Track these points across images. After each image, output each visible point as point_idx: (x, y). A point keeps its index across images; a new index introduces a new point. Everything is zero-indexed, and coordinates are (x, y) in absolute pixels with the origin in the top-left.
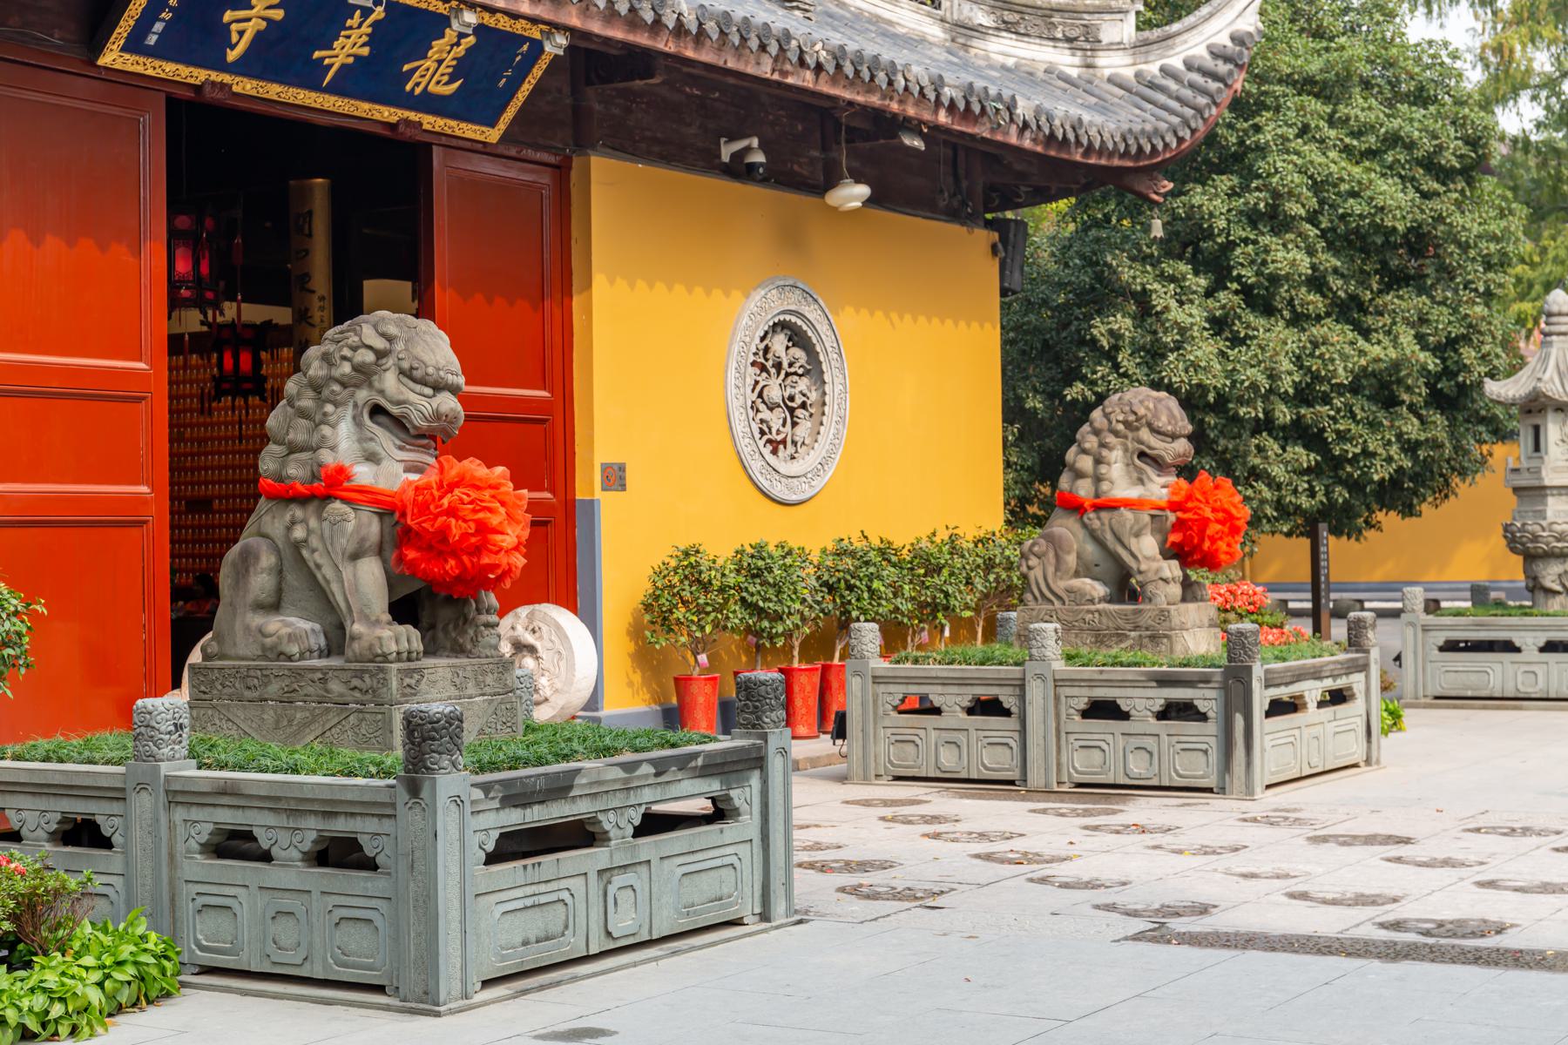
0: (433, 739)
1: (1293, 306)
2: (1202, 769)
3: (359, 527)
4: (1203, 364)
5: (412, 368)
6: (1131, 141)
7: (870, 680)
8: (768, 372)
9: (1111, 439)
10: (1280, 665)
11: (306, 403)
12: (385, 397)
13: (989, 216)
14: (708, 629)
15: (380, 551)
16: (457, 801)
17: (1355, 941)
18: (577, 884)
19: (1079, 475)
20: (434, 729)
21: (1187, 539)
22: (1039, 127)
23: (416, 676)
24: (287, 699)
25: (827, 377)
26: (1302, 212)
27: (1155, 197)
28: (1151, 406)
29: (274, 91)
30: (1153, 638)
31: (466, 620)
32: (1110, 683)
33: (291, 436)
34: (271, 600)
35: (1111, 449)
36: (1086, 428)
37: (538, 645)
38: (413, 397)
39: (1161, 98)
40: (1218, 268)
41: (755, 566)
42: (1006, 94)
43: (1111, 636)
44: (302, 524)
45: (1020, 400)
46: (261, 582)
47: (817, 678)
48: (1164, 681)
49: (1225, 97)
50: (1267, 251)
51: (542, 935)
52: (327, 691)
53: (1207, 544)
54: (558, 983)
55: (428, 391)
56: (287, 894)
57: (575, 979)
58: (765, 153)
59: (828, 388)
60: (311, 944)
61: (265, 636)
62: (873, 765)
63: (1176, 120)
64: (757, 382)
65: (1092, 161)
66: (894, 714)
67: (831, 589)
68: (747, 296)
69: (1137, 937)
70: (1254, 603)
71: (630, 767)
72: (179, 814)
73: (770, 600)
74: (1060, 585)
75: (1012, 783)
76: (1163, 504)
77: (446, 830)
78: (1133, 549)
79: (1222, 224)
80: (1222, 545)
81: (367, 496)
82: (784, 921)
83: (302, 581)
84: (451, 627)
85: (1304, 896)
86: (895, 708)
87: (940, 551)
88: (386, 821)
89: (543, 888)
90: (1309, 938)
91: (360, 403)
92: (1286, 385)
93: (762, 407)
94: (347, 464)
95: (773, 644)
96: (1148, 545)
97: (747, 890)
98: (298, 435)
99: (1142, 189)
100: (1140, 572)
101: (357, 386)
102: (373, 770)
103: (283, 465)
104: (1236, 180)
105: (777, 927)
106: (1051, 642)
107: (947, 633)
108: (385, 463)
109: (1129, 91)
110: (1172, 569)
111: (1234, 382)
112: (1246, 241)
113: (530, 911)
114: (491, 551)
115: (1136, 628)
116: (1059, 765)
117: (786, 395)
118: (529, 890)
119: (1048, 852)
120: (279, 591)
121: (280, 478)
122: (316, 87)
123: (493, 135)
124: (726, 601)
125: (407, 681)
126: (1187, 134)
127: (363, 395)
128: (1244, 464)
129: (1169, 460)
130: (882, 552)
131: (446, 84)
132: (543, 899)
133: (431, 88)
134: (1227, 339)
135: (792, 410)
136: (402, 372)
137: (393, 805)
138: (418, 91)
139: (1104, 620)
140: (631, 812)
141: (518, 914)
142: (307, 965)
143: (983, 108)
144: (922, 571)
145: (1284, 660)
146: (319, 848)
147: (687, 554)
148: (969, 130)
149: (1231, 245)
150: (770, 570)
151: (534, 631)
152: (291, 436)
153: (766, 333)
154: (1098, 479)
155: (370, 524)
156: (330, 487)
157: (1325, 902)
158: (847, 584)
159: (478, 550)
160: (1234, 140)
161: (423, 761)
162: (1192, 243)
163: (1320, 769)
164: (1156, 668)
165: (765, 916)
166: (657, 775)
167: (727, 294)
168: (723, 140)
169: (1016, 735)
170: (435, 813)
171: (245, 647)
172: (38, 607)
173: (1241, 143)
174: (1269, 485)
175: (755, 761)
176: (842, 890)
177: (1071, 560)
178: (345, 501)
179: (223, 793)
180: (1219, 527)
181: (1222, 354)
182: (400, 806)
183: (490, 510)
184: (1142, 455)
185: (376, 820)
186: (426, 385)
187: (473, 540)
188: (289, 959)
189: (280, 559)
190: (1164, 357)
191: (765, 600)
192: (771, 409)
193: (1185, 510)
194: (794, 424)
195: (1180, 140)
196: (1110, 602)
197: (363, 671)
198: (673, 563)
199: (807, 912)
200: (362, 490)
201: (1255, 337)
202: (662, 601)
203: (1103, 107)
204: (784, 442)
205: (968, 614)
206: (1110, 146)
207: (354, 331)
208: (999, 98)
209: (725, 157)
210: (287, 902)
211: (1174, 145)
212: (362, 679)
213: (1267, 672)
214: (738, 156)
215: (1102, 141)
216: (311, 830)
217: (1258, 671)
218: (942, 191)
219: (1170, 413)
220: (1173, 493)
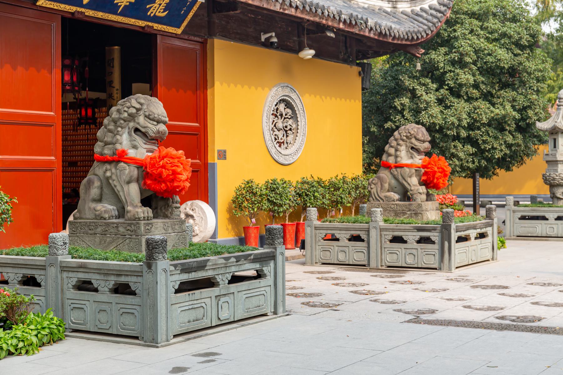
0: (156, 248)
2: (433, 261)
3: (130, 172)
4: (435, 115)
5: (149, 115)
6: (409, 35)
7: (314, 228)
9: (401, 142)
10: (461, 224)
11: (111, 127)
13: (358, 62)
14: (256, 210)
15: (137, 181)
16: (165, 271)
17: (487, 323)
18: (208, 301)
19: (389, 155)
20: (157, 245)
22: (376, 29)
23: (150, 226)
24: (104, 234)
25: (299, 119)
26: (471, 61)
27: (418, 55)
29: (100, 15)
30: (416, 214)
32: (400, 230)
34: (98, 198)
35: (401, 146)
36: (392, 138)
37: (194, 215)
40: (440, 81)
41: (272, 187)
42: (364, 17)
43: (401, 213)
44: (109, 171)
45: (369, 128)
46: (95, 192)
47: (294, 228)
48: (419, 229)
49: (444, 19)
50: (458, 75)
51: (195, 319)
52: (118, 231)
53: (435, 181)
54: (201, 336)
55: (155, 123)
56: (104, 304)
57: (207, 335)
59: (299, 123)
60: (112, 322)
61: (96, 211)
63: (426, 27)
64: (274, 121)
65: (395, 42)
66: (322, 241)
67: (300, 195)
68: (270, 90)
69: (409, 321)
70: (452, 202)
71: (227, 259)
72: (65, 275)
73: (278, 199)
74: (382, 195)
75: (364, 266)
76: (420, 166)
79: (442, 65)
80: (441, 181)
81: (133, 161)
82: (282, 314)
83: (109, 191)
84: (163, 208)
85: (469, 307)
86: (323, 238)
87: (339, 182)
88: (139, 278)
89: (195, 302)
90: (471, 322)
91: (131, 127)
92: (465, 123)
93: (275, 130)
96: (414, 181)
97: (269, 303)
98: (108, 139)
99: (413, 52)
100: (411, 190)
101: (130, 121)
103: (103, 149)
104: (447, 49)
105: (280, 317)
107: (341, 212)
108: (139, 149)
109: (409, 16)
110: (423, 189)
111: (446, 122)
112: (450, 71)
113: (191, 311)
115: (410, 210)
116: (381, 259)
118: (191, 303)
119: (377, 291)
120: (101, 195)
123: (179, 31)
124: (262, 199)
125: (147, 227)
126: (429, 32)
127: (132, 124)
128: (449, 152)
129: (422, 150)
130: (318, 182)
131: (162, 12)
132: (195, 306)
133: (157, 14)
134: (443, 106)
135: (286, 131)
136: (146, 116)
137: (142, 272)
138: (152, 15)
139: (398, 207)
140: (227, 275)
143: (356, 22)
144: (333, 189)
145: (463, 222)
146: (115, 287)
147: (248, 183)
148: (351, 30)
149: (445, 73)
150: (278, 189)
151: (193, 210)
152: (106, 139)
153: (277, 103)
154: (396, 157)
155: (134, 171)
156: (120, 157)
157: (477, 309)
158: (306, 194)
159: (173, 181)
161: (153, 256)
164: (417, 225)
165: (275, 313)
166: (237, 262)
167: (263, 89)
168: (262, 33)
169: (366, 249)
173: (449, 36)
174: (458, 160)
175: (272, 257)
176: (303, 303)
177: (386, 186)
179: (81, 267)
180: (440, 174)
181: (442, 112)
182: (144, 272)
183: (177, 166)
185: (136, 277)
187: (171, 177)
188: (104, 327)
190: (421, 113)
191: (276, 199)
192: (279, 131)
193: (428, 168)
194: (287, 136)
195: (427, 35)
196: (400, 201)
197: (132, 224)
198: (243, 186)
199: (290, 311)
200: (131, 159)
201: (452, 106)
203: (399, 22)
204: (283, 142)
205: (349, 205)
206: (402, 37)
208: (362, 19)
209: (263, 39)
210: (104, 307)
211: (425, 36)
213: (457, 226)
214: (267, 39)
216: (112, 281)
217: (453, 226)
218: (341, 52)
219: (422, 133)
220: (423, 162)
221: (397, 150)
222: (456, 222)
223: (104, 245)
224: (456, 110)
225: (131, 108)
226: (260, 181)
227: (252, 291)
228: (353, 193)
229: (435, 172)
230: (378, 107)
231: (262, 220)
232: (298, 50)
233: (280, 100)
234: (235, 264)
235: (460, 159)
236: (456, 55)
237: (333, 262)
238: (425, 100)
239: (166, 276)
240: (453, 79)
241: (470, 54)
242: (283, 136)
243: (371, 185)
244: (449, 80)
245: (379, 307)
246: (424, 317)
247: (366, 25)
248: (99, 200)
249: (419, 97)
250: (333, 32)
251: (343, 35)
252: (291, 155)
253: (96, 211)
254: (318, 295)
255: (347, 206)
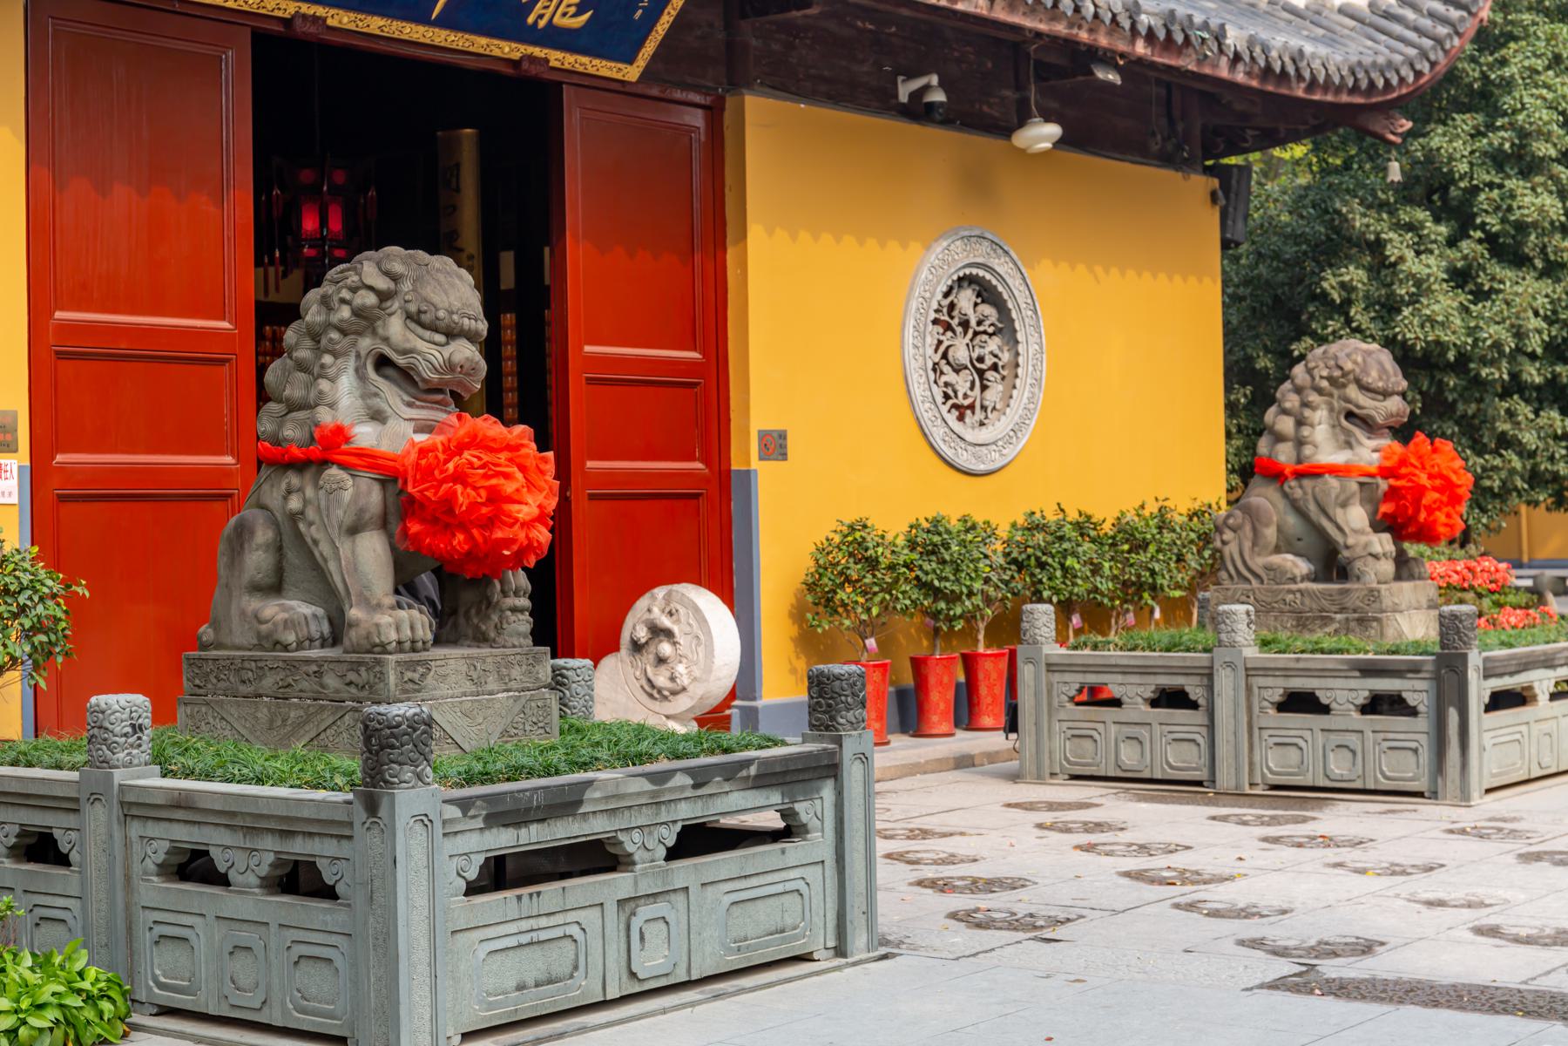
0: (392, 747)
1: (1546, 254)
2: (1411, 770)
3: (356, 496)
4: (1440, 318)
5: (420, 312)
6: (1361, 75)
7: (1044, 668)
8: (954, 331)
9: (1313, 397)
10: (1505, 652)
11: (303, 353)
12: (389, 346)
13: (1210, 163)
14: (875, 611)
15: (384, 524)
16: (424, 820)
17: (1539, 994)
18: (591, 917)
19: (1279, 438)
20: (393, 735)
21: (1400, 509)
22: (1252, 58)
23: (421, 670)
24: (282, 695)
25: (1020, 336)
26: (1553, 153)
27: (1392, 137)
28: (1359, 359)
29: (374, 24)
30: (1362, 621)
31: (489, 604)
32: (1307, 672)
33: (287, 392)
34: (269, 581)
35: (1314, 408)
36: (1287, 385)
37: (676, 629)
38: (422, 346)
39: (1397, 28)
40: (1461, 218)
41: (931, 542)
42: (1214, 23)
43: (1315, 618)
44: (285, 494)
45: (1250, 360)
46: (257, 561)
47: (1003, 664)
48: (1369, 670)
49: (1470, 27)
50: (1513, 196)
51: (543, 977)
52: (323, 686)
53: (1423, 516)
54: (561, 1035)
55: (440, 338)
56: (245, 925)
57: (584, 1030)
58: (947, 92)
59: (1021, 348)
60: (269, 987)
61: (261, 622)
62: (1047, 762)
63: (1412, 52)
64: (940, 342)
65: (1317, 97)
66: (1070, 706)
67: (1021, 566)
68: (928, 248)
69: (1274, 986)
70: (1495, 582)
71: (660, 778)
72: (135, 829)
73: (947, 579)
74: (1258, 562)
75: (1199, 783)
76: (1373, 470)
77: (408, 855)
78: (1340, 521)
79: (1463, 167)
80: (1441, 517)
81: (368, 461)
82: (864, 956)
83: (297, 563)
84: (473, 611)
85: (1493, 932)
86: (1072, 699)
87: (1147, 525)
88: (344, 843)
89: (543, 922)
90: (1484, 989)
91: (363, 353)
92: (1535, 344)
93: (946, 369)
94: (346, 423)
95: (951, 628)
96: (1356, 517)
97: (818, 920)
98: (294, 391)
99: (1377, 128)
100: (1347, 547)
101: (359, 334)
102: (339, 780)
103: (281, 426)
104: (1480, 118)
105: (854, 964)
106: (1242, 626)
107: (1157, 615)
108: (391, 422)
109: (1361, 21)
110: (1383, 543)
111: (1476, 340)
112: (1491, 185)
113: (527, 950)
114: (505, 524)
115: (1342, 610)
116: (1251, 764)
117: (975, 356)
118: (525, 925)
119: (1209, 869)
120: (279, 571)
121: (276, 441)
122: (423, 19)
123: (632, 73)
124: (896, 581)
125: (409, 675)
126: (1426, 68)
127: (366, 343)
128: (1494, 429)
129: (1380, 420)
130: (1078, 526)
131: (574, 16)
132: (543, 936)
133: (556, 20)
134: (1471, 292)
135: (981, 373)
136: (409, 316)
137: (351, 824)
138: (542, 23)
139: (1307, 601)
140: (663, 831)
141: (511, 953)
142: (266, 1010)
143: (1187, 38)
144: (1126, 547)
145: (1511, 646)
146: (279, 872)
147: (852, 528)
148: (1173, 62)
149: (1475, 190)
150: (947, 547)
151: (671, 614)
152: (287, 392)
153: (951, 289)
154: (1300, 443)
155: (369, 492)
156: (329, 450)
157: (1517, 940)
158: (1038, 558)
159: (491, 522)
160: (1477, 75)
161: (381, 773)
162: (1433, 189)
163: (1553, 770)
164: (1361, 656)
165: (840, 951)
166: (696, 786)
167: (904, 246)
168: (900, 78)
169: (1204, 731)
170: (394, 835)
171: (241, 634)
172: (80, 590)
173: (1485, 76)
174: (1520, 454)
175: (827, 768)
176: (953, 916)
177: (1270, 533)
178: (344, 466)
179: (177, 806)
180: (1436, 495)
181: (1465, 309)
182: (357, 825)
183: (507, 476)
184: (1350, 415)
185: (335, 841)
186: (436, 331)
187: (484, 510)
188: (247, 1002)
189: (279, 533)
190: (1399, 311)
191: (940, 579)
192: (957, 371)
193: (1398, 477)
194: (984, 388)
195: (1418, 74)
196: (1315, 580)
197: (360, 663)
198: (837, 539)
199: (899, 944)
200: (361, 454)
201: (1499, 291)
202: (825, 580)
203: (1332, 37)
204: (972, 407)
205: (1177, 594)
206: (1337, 80)
207: (355, 269)
208: (1205, 26)
209: (903, 97)
210: (246, 936)
211: (1411, 79)
212: (358, 672)
213: (1486, 660)
214: (917, 95)
215: (1327, 75)
216: (269, 849)
217: (1475, 659)
218: (1154, 134)
219: (1379, 364)
220: (1386, 458)
221: (1300, 423)
222: (1485, 647)
223: (283, 731)
224: (1508, 303)
225: (363, 292)
226: (892, 524)
227: (754, 882)
228: (1189, 556)
229: (1420, 490)
230: (1276, 299)
231: (903, 641)
232: (1005, 129)
233: (960, 279)
234: (689, 793)
235: (1527, 454)
236: (1506, 135)
237: (1102, 773)
238: (1413, 276)
239: (428, 845)
240: (1498, 208)
241: (1550, 133)
242: (972, 388)
243: (1221, 534)
244: (1486, 212)
245: (1199, 928)
246: (1332, 969)
247: (1220, 45)
248: (275, 587)
249: (1394, 265)
250: (1117, 68)
251: (1158, 82)
252: (994, 443)
253: (261, 622)
254: (1014, 884)
255: (1169, 598)
